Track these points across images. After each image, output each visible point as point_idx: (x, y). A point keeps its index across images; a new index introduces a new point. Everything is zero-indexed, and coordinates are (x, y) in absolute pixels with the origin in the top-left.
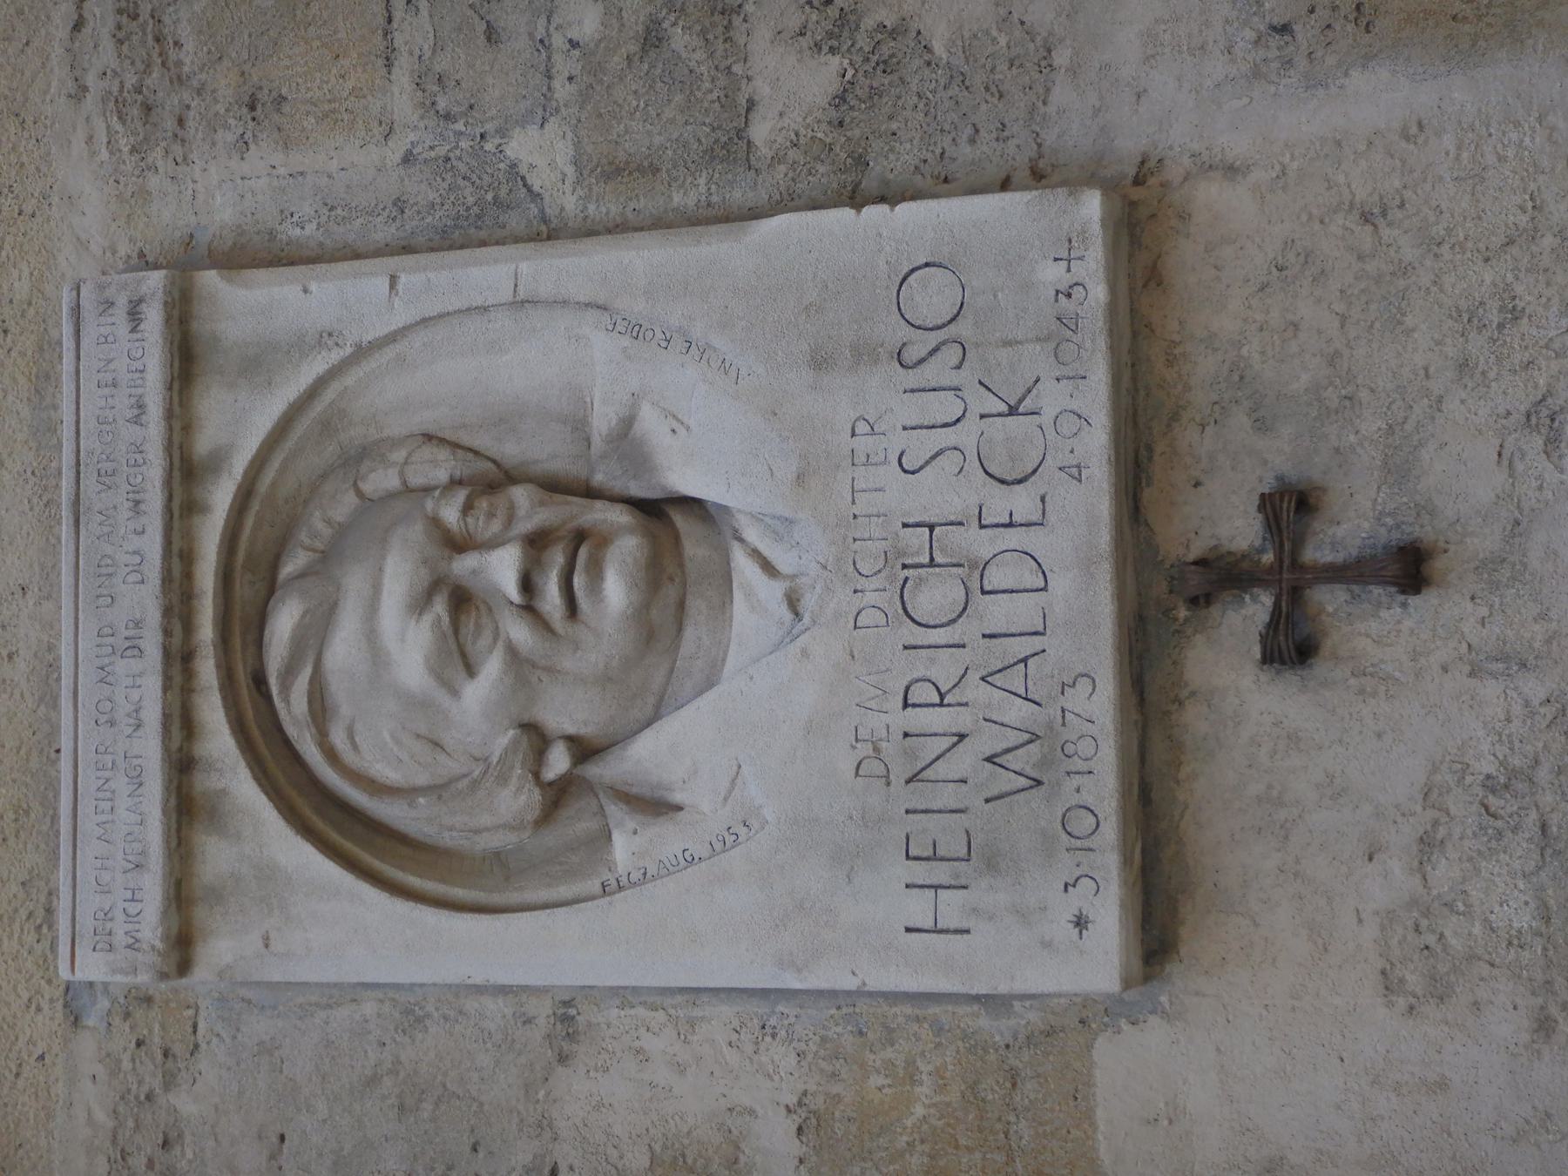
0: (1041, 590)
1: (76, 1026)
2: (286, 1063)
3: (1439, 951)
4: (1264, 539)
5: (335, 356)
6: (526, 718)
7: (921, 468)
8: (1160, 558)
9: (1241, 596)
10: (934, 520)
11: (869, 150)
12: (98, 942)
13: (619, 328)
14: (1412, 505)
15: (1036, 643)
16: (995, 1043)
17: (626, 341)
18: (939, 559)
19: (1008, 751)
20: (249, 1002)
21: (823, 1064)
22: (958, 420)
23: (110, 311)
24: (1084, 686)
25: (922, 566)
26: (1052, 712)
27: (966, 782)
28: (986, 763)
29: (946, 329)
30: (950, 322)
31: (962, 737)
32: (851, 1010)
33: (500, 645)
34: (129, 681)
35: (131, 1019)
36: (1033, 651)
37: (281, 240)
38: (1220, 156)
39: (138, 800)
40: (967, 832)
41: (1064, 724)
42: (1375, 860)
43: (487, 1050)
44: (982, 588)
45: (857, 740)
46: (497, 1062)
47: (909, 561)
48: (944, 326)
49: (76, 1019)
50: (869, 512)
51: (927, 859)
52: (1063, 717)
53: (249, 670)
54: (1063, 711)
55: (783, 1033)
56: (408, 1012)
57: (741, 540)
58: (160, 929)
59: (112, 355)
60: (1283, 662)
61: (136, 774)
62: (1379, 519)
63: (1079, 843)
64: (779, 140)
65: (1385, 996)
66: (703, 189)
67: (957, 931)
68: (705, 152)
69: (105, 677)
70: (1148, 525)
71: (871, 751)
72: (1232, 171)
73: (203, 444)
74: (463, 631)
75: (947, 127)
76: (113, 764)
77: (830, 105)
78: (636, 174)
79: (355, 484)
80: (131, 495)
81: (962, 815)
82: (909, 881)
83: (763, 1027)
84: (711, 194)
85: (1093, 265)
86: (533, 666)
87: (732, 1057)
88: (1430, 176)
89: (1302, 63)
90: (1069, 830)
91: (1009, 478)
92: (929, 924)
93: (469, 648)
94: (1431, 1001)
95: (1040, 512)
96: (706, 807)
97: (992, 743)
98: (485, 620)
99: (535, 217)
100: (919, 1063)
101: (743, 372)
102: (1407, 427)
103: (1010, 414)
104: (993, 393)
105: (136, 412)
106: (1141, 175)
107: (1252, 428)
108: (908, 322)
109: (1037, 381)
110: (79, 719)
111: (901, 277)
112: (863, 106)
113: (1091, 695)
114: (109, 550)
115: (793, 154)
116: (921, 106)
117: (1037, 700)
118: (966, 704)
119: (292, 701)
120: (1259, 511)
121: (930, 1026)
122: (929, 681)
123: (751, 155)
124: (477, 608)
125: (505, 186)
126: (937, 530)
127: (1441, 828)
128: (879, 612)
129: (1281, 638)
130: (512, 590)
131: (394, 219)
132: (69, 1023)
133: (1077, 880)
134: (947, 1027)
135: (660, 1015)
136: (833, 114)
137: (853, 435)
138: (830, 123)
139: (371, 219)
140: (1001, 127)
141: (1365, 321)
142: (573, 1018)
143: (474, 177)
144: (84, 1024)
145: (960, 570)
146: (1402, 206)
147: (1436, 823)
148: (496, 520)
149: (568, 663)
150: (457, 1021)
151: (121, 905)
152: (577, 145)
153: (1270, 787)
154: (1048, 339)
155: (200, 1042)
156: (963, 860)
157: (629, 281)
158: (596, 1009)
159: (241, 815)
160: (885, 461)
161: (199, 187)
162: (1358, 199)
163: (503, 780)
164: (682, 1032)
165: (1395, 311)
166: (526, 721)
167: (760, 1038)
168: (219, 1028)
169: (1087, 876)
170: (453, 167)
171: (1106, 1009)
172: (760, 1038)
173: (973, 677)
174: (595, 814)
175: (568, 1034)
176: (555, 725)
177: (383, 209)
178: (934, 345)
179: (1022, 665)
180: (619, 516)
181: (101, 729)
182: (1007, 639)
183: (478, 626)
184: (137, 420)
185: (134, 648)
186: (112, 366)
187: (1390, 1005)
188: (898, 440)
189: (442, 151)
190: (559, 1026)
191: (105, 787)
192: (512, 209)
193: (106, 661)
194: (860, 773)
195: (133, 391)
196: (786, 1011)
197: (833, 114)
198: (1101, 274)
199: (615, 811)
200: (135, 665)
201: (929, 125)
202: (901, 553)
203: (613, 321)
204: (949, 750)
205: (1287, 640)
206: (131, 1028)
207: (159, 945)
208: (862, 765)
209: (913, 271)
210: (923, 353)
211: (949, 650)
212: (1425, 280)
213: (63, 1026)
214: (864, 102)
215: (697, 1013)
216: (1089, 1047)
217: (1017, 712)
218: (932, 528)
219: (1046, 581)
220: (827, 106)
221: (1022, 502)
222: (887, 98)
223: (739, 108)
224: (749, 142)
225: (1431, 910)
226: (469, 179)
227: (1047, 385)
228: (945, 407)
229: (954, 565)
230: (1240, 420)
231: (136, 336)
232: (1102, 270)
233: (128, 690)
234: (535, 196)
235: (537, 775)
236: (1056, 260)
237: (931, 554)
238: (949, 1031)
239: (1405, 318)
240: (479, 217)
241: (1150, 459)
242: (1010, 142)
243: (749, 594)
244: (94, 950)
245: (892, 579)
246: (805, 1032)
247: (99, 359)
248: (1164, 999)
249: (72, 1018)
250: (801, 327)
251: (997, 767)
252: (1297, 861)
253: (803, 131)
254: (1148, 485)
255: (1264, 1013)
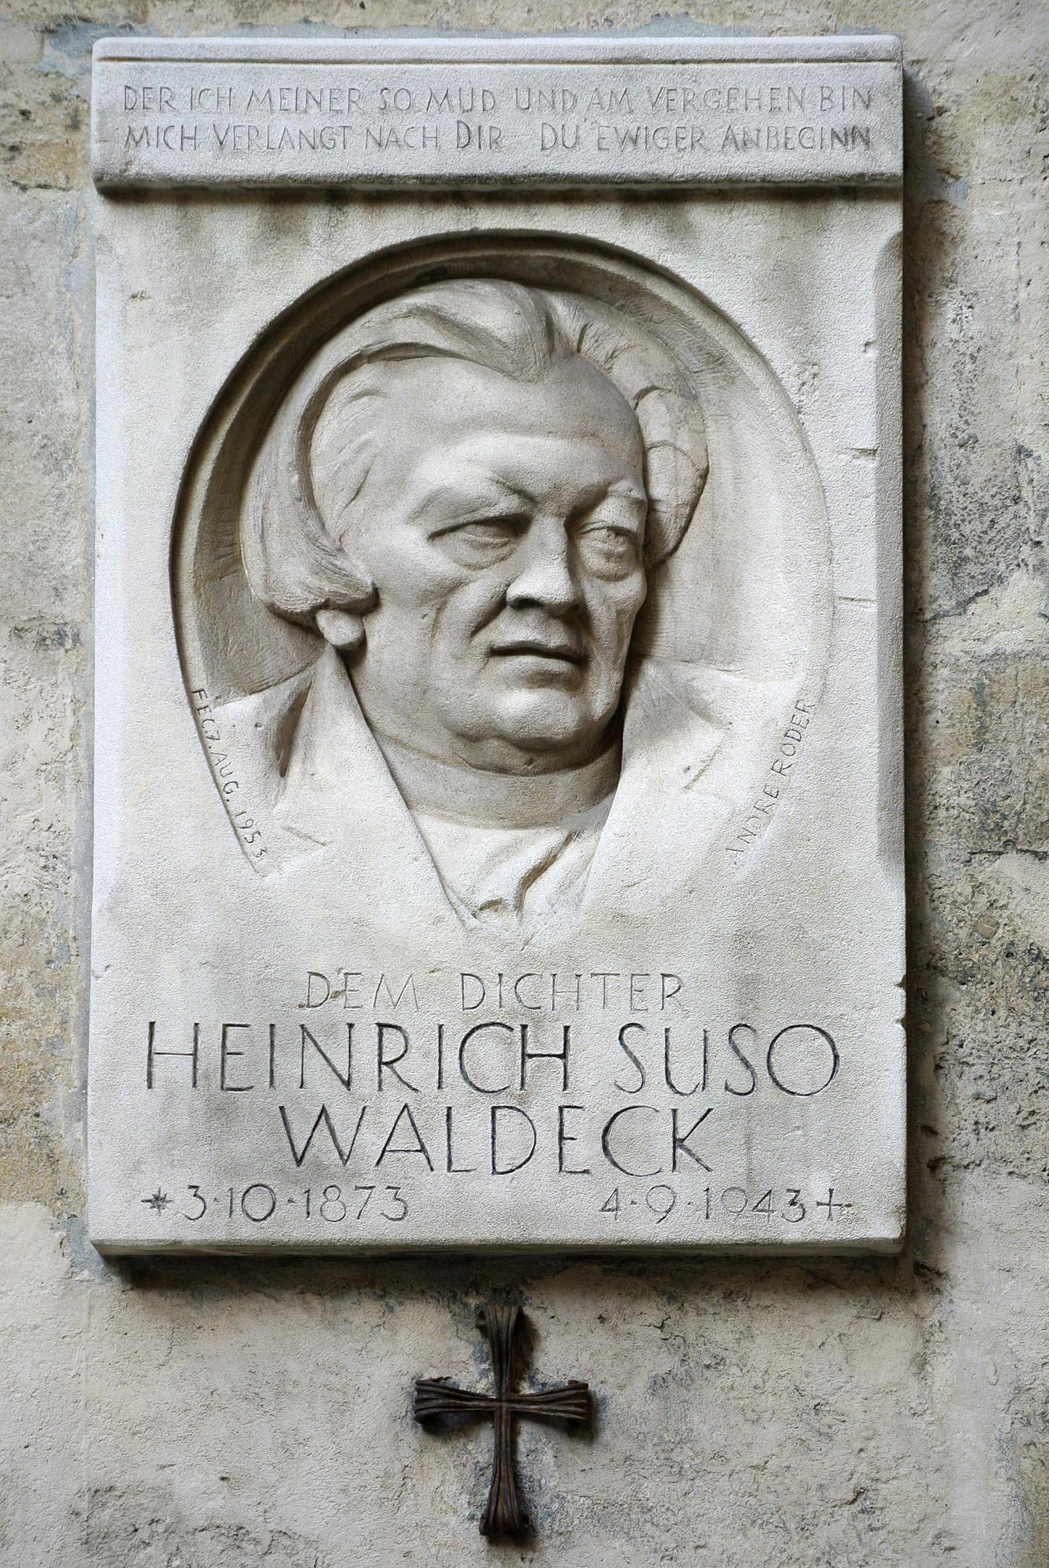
0: (494, 1168)
1: (42, 32)
2: (7, 301)
3: (133, 1541)
4: (544, 1385)
5: (790, 382)
6: (384, 596)
7: (625, 1047)
8: (529, 1281)
9: (488, 1359)
10: (570, 1058)
11: (979, 986)
12: (135, 92)
13: (799, 715)
14: (570, 1529)
15: (440, 1161)
16: (40, 1102)
17: (783, 723)
18: (530, 1063)
19: (332, 1131)
20: (74, 256)
21: (17, 921)
22: (672, 1086)
23: (859, 105)
24: (396, 1209)
25: (524, 1047)
26: (371, 1176)
27: (301, 1087)
28: (321, 1108)
29: (768, 1076)
30: (775, 1080)
31: (348, 1084)
32: (73, 952)
33: (465, 572)
34: (431, 133)
35: (53, 103)
36: (431, 1158)
37: (941, 294)
38: (938, 1351)
39: (296, 143)
40: (251, 1088)
41: (357, 1188)
42: (222, 1482)
43: (25, 545)
44: (499, 1107)
45: (346, 974)
46: (12, 557)
47: (529, 1032)
48: (771, 1073)
49: (52, 32)
50: (582, 991)
51: (224, 1046)
52: (365, 1188)
53: (447, 265)
54: (371, 1188)
55: (49, 879)
56: (66, 452)
57: (567, 841)
58: (150, 172)
59: (808, 106)
60: (418, 1401)
61: (325, 139)
62: (558, 1497)
63: (238, 1201)
64: (999, 888)
65: (89, 1490)
66: (955, 800)
67: (150, 1074)
68: (994, 804)
69: (440, 99)
70: (564, 1269)
71: (335, 989)
72: (921, 1364)
73: (700, 216)
74: (480, 529)
75: (995, 1069)
76: (337, 111)
77: (1032, 944)
78: (977, 725)
79: (653, 388)
80: (643, 132)
81: (267, 1084)
82: (201, 1027)
83: (54, 857)
84: (947, 809)
85: (821, 1228)
86: (439, 609)
87: (23, 822)
88: (898, 1556)
89: (1024, 1436)
90: (252, 1191)
91: (609, 1138)
92: (157, 1047)
93: (461, 535)
94: (84, 1533)
95: (573, 1170)
96: (282, 806)
97: (343, 1115)
98: (491, 554)
99: (940, 606)
100: (19, 1022)
101: (740, 856)
102: (649, 1525)
103: (675, 1140)
104: (698, 1124)
105: (740, 138)
106: (925, 1271)
107: (656, 1375)
108: (778, 1036)
109: (707, 1168)
110: (389, 66)
111: (825, 1029)
112: (1028, 980)
113: (386, 1216)
114: (583, 104)
115: (982, 900)
116: (1021, 1042)
117: (382, 1162)
118: (380, 1089)
119: (408, 321)
120: (571, 1382)
121: (57, 1036)
122: (406, 1051)
123: (986, 855)
124: (505, 544)
125: (979, 571)
126: (560, 1062)
127: (252, 1546)
128: (478, 999)
129: (440, 1401)
130: (517, 590)
131: (954, 436)
132: (47, 23)
133: (200, 1198)
134: (56, 1053)
135: (66, 744)
136: (1022, 947)
137: (664, 975)
138: (1012, 943)
139: (957, 406)
140: (990, 1127)
141: (757, 1490)
142: (62, 644)
143: (992, 534)
144: (47, 42)
145: (518, 1085)
146: (871, 1529)
147: (257, 1542)
148: (603, 562)
149: (444, 646)
150: (57, 510)
151: (177, 122)
152: (1017, 657)
153: (296, 1384)
154: (750, 1180)
155: (28, 192)
156: (223, 1082)
157: (847, 731)
158: (72, 671)
159: (280, 265)
160: (634, 1009)
161: (1015, 187)
162: (881, 1486)
163: (319, 570)
164: (49, 767)
165: (765, 1518)
166: (382, 596)
167: (43, 853)
168: (45, 217)
169: (205, 1208)
170: (1007, 507)
171: (75, 1216)
172: (43, 853)
173: (408, 1097)
174: (280, 671)
175: (44, 639)
176: (378, 628)
177: (966, 422)
178: (752, 1063)
179: (419, 1148)
180: (601, 699)
181: (377, 96)
182: (446, 1132)
183: (485, 546)
184: (730, 139)
185: (468, 138)
186: (794, 106)
187: (80, 1494)
188: (655, 1024)
189: (1026, 494)
190: (53, 628)
191: (311, 102)
192: (952, 579)
193: (455, 102)
194: (313, 977)
195: (764, 135)
196: (72, 881)
197: (1022, 947)
198: (810, 1237)
199: (281, 696)
200: (449, 140)
201: (999, 1050)
202: (538, 1023)
203: (807, 709)
204: (334, 1070)
205: (438, 1407)
206: (43, 103)
207: (133, 171)
208: (321, 979)
209: (831, 1042)
210: (745, 1052)
211: (437, 1073)
212: (794, 1550)
213: (44, 14)
214: (1031, 981)
215: (69, 784)
216: (37, 1199)
217: (371, 1142)
218: (563, 1056)
219: (502, 1173)
220: (1031, 941)
221: (583, 1151)
222: (1033, 1007)
223: (1038, 843)
224: (1000, 854)
225: (173, 1535)
226: (991, 527)
227: (703, 1178)
228: (687, 1072)
229: (523, 1079)
230: (666, 1362)
231: (828, 136)
232: (817, 1238)
233: (421, 130)
234: (963, 605)
235: (325, 606)
236: (831, 1191)
237: (536, 1055)
238: (52, 1055)
239: (757, 1528)
240: (947, 539)
241: (630, 1273)
242: (973, 1136)
243: (509, 851)
244: (127, 87)
245: (513, 1014)
246: (50, 903)
247: (804, 90)
248: (86, 1274)
249: (52, 26)
250: (781, 922)
251: (316, 1119)
252: (221, 1408)
253: (1006, 913)
254: (604, 1270)
255: (72, 1373)
